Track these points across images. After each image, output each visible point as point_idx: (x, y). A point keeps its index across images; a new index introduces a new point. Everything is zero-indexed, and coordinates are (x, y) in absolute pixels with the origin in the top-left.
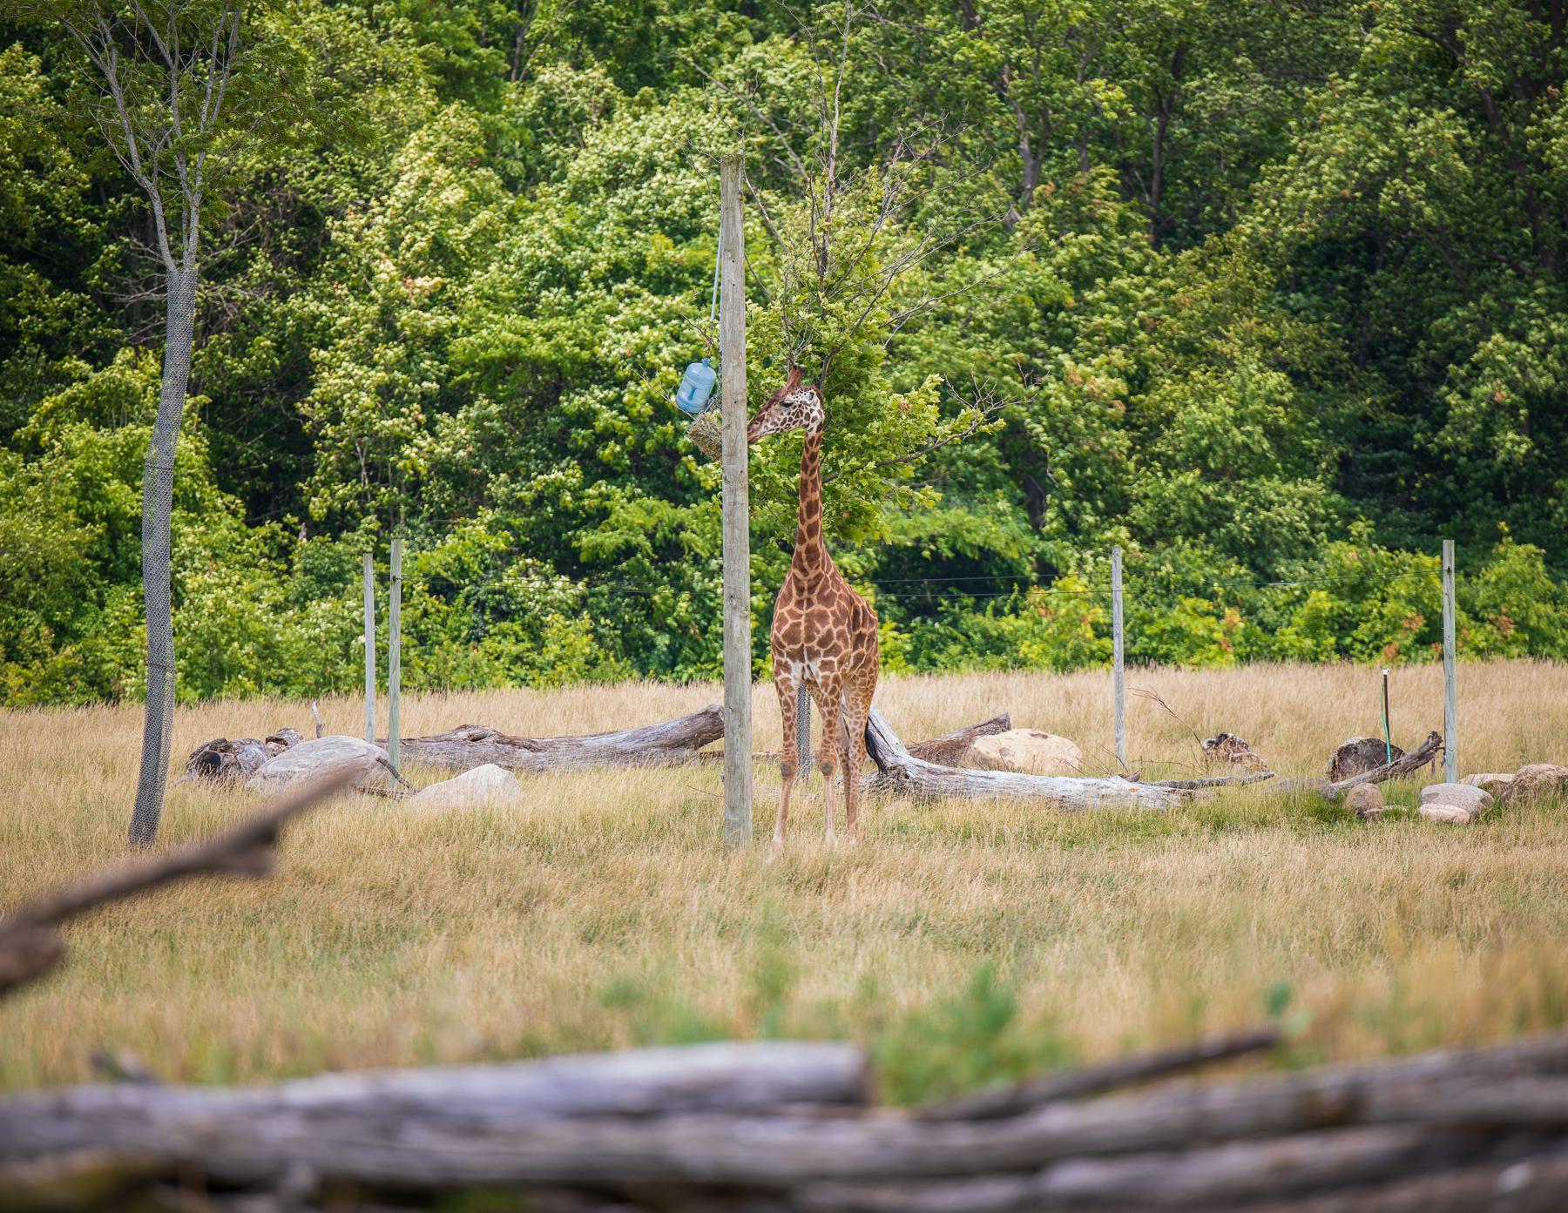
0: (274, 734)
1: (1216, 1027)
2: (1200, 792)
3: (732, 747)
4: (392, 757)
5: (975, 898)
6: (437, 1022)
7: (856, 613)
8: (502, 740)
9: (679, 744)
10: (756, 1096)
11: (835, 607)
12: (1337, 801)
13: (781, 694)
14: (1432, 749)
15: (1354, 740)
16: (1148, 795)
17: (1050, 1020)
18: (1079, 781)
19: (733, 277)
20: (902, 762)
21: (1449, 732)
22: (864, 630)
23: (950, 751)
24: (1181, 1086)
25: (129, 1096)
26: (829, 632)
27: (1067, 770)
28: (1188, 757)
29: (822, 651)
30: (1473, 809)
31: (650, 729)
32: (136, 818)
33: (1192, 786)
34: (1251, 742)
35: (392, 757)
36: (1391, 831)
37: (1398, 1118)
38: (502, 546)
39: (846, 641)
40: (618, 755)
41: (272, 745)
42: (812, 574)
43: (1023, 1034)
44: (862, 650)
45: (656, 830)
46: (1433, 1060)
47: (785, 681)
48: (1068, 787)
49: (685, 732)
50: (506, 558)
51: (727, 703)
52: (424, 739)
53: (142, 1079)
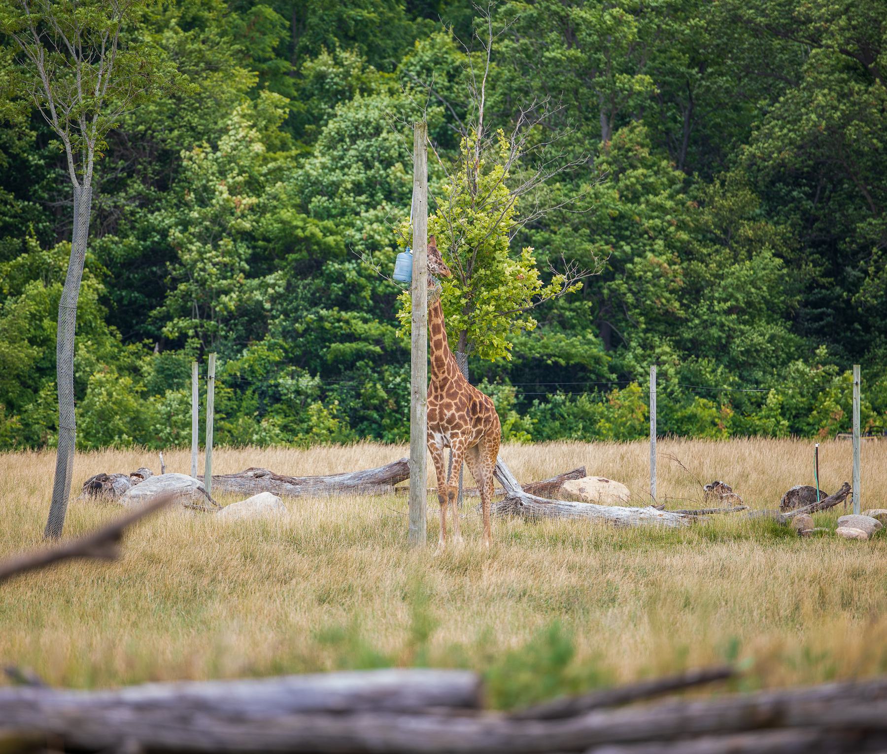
0: (136, 471)
1: (695, 664)
2: (700, 517)
3: (414, 485)
4: (207, 486)
5: (562, 580)
6: (220, 651)
7: (475, 405)
8: (275, 478)
9: (384, 481)
10: (411, 702)
11: (457, 400)
12: (785, 524)
13: (432, 453)
14: (844, 494)
15: (797, 487)
16: (669, 518)
17: (598, 656)
18: (628, 509)
19: (420, 197)
20: (519, 495)
21: (855, 483)
22: (481, 415)
23: (549, 489)
24: (672, 701)
25: (28, 694)
26: (453, 415)
27: (619, 502)
28: (694, 496)
29: (450, 427)
30: (869, 530)
31: (365, 472)
32: (50, 522)
33: (696, 513)
34: (733, 487)
35: (207, 486)
36: (818, 543)
37: (806, 724)
38: (277, 358)
39: (465, 421)
40: (344, 488)
41: (134, 478)
42: (441, 376)
43: (575, 668)
44: (481, 427)
45: (367, 535)
46: (829, 688)
47: (432, 444)
48: (620, 512)
49: (387, 475)
50: (280, 365)
51: (412, 457)
52: (227, 476)
53: (35, 683)
